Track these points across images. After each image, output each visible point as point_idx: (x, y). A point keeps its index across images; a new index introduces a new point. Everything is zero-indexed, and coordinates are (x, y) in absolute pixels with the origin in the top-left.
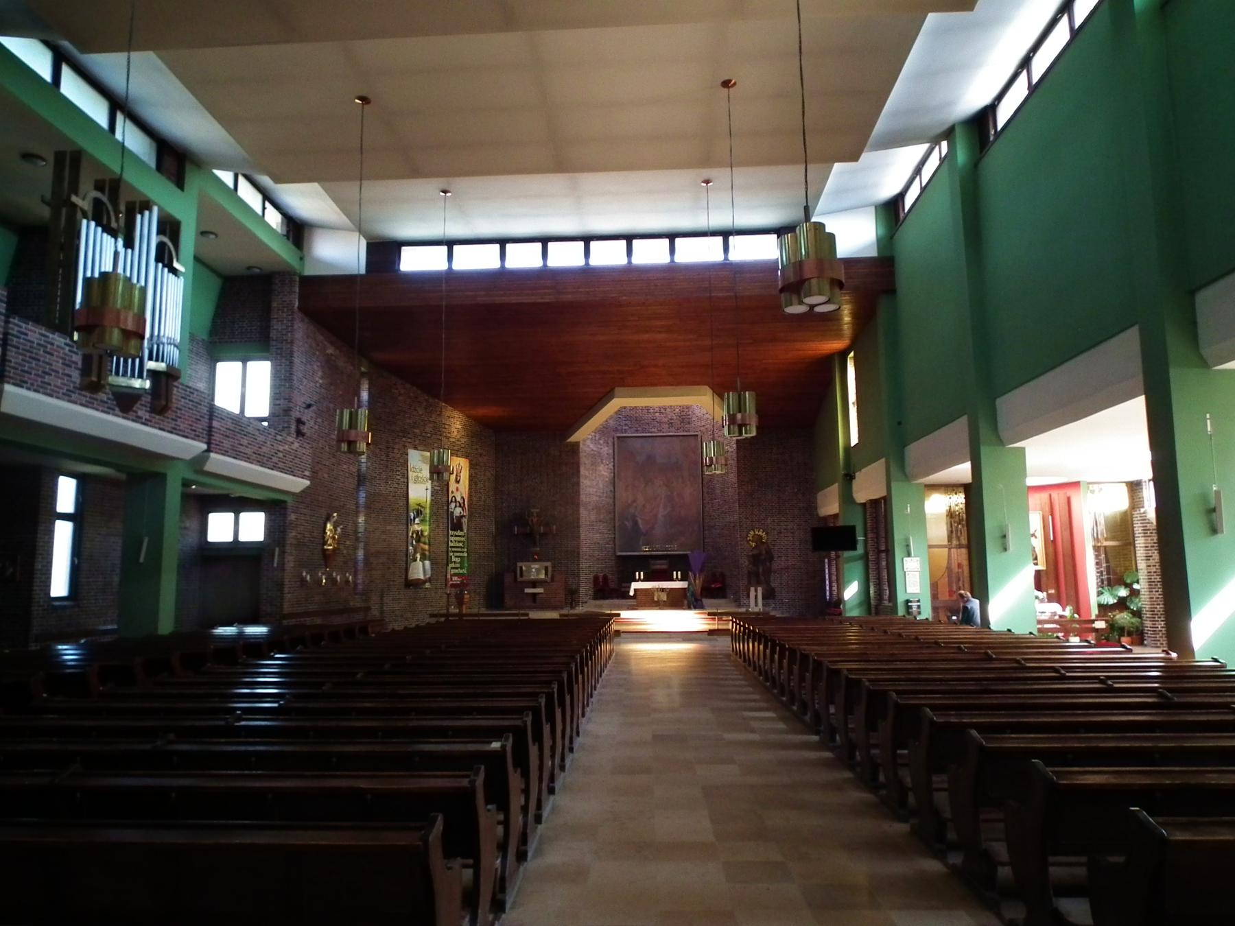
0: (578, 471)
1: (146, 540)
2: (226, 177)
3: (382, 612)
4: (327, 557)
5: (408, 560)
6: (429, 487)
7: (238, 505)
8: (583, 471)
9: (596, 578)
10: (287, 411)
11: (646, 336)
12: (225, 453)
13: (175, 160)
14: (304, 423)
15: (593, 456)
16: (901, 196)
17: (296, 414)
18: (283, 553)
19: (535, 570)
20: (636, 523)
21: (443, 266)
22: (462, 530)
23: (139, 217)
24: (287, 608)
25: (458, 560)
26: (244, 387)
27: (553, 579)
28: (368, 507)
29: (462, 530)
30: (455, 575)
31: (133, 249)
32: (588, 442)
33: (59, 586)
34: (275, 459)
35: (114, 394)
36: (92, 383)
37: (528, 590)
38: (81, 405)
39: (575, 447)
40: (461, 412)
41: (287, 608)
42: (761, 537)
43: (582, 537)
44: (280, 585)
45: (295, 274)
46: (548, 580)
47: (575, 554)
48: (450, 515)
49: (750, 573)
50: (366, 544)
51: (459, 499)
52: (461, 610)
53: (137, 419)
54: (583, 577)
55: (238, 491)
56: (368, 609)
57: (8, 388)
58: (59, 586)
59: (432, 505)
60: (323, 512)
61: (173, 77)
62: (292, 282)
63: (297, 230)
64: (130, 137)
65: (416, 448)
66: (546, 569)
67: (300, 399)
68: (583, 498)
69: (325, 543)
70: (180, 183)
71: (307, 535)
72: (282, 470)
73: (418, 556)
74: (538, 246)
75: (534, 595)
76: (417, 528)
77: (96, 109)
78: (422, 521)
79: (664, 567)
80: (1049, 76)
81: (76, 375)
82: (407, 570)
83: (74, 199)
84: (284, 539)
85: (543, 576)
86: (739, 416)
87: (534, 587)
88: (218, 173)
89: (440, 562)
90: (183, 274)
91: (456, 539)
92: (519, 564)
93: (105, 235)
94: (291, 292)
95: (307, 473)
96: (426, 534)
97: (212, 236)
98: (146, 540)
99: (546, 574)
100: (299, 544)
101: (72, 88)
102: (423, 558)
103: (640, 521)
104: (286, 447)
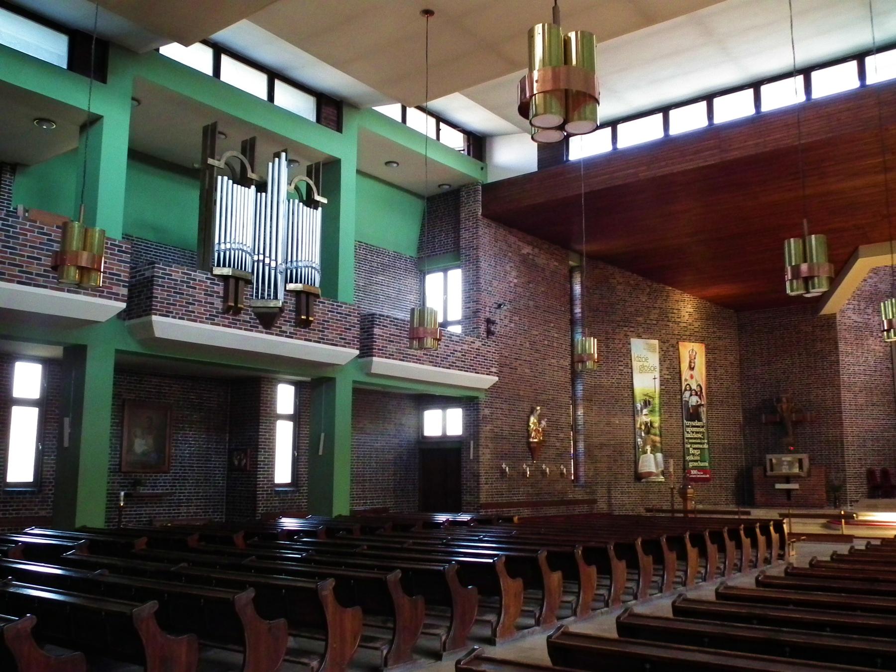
0: (837, 348)
1: (323, 435)
2: (392, 111)
3: (610, 505)
4: (532, 450)
5: (636, 452)
6: (657, 375)
7: (444, 401)
8: (842, 346)
9: (871, 474)
10: (476, 312)
11: (859, 182)
12: (391, 356)
13: (332, 109)
14: (493, 323)
15: (858, 329)
17: (483, 316)
18: (477, 446)
19: (786, 463)
22: (700, 420)
23: (270, 164)
24: (483, 498)
25: (697, 452)
26: (445, 294)
27: (809, 474)
28: (588, 399)
29: (700, 420)
30: (694, 468)
31: (266, 192)
32: (849, 313)
33: (283, 473)
34: (451, 359)
35: (256, 314)
36: (231, 311)
37: (778, 486)
38: (224, 326)
40: (691, 293)
41: (483, 498)
43: (847, 423)
44: (477, 476)
45: (477, 183)
47: (838, 443)
48: (684, 405)
50: (587, 437)
51: (694, 387)
52: (685, 505)
53: (282, 333)
54: (850, 471)
55: (438, 391)
56: (594, 501)
57: (155, 318)
58: (283, 473)
59: (661, 395)
60: (526, 406)
61: (283, 41)
62: (476, 191)
63: (478, 144)
64: (288, 98)
65: (639, 337)
66: (800, 461)
67: (489, 301)
68: (845, 378)
69: (529, 436)
70: (339, 128)
71: (506, 428)
72: (461, 369)
73: (649, 448)
75: (788, 491)
76: (647, 419)
77: (254, 83)
78: (652, 412)
81: (218, 303)
82: (636, 463)
83: (210, 161)
84: (478, 432)
85: (796, 470)
86: (804, 267)
87: (788, 482)
88: (380, 109)
89: (673, 451)
90: (323, 205)
91: (692, 430)
92: (769, 456)
93: (235, 185)
94: (476, 201)
95: (494, 370)
96: (656, 425)
97: (395, 165)
98: (323, 435)
99: (801, 467)
100: (496, 437)
101: (233, 73)
102: (654, 451)
104: (465, 347)
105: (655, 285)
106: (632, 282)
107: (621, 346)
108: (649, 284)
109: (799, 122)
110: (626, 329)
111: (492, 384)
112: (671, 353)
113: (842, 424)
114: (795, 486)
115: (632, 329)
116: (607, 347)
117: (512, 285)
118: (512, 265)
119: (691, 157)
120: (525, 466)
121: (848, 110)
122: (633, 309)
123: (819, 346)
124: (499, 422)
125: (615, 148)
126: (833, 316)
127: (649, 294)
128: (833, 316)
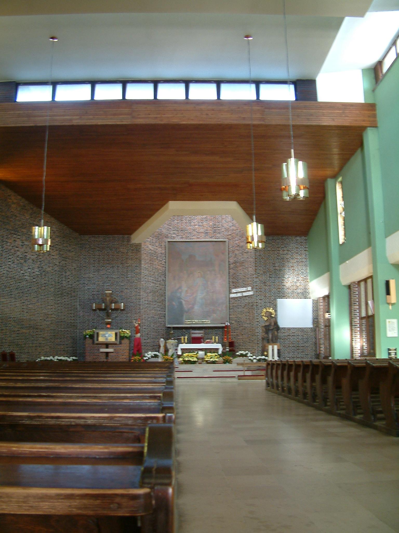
0: (140, 264)
11: (312, 111)
16: (380, 63)
20: (181, 303)
21: (214, 97)
39: (137, 248)
42: (271, 314)
46: (118, 342)
49: (263, 339)
74: (253, 86)
75: (107, 353)
79: (199, 335)
80: (392, 69)
87: (107, 347)
103: (184, 302)
106: (21, 204)
108: (32, 207)
109: (249, 60)
110: (15, 236)
112: (41, 257)
115: (19, 237)
122: (20, 223)
123: (130, 262)
127: (31, 214)
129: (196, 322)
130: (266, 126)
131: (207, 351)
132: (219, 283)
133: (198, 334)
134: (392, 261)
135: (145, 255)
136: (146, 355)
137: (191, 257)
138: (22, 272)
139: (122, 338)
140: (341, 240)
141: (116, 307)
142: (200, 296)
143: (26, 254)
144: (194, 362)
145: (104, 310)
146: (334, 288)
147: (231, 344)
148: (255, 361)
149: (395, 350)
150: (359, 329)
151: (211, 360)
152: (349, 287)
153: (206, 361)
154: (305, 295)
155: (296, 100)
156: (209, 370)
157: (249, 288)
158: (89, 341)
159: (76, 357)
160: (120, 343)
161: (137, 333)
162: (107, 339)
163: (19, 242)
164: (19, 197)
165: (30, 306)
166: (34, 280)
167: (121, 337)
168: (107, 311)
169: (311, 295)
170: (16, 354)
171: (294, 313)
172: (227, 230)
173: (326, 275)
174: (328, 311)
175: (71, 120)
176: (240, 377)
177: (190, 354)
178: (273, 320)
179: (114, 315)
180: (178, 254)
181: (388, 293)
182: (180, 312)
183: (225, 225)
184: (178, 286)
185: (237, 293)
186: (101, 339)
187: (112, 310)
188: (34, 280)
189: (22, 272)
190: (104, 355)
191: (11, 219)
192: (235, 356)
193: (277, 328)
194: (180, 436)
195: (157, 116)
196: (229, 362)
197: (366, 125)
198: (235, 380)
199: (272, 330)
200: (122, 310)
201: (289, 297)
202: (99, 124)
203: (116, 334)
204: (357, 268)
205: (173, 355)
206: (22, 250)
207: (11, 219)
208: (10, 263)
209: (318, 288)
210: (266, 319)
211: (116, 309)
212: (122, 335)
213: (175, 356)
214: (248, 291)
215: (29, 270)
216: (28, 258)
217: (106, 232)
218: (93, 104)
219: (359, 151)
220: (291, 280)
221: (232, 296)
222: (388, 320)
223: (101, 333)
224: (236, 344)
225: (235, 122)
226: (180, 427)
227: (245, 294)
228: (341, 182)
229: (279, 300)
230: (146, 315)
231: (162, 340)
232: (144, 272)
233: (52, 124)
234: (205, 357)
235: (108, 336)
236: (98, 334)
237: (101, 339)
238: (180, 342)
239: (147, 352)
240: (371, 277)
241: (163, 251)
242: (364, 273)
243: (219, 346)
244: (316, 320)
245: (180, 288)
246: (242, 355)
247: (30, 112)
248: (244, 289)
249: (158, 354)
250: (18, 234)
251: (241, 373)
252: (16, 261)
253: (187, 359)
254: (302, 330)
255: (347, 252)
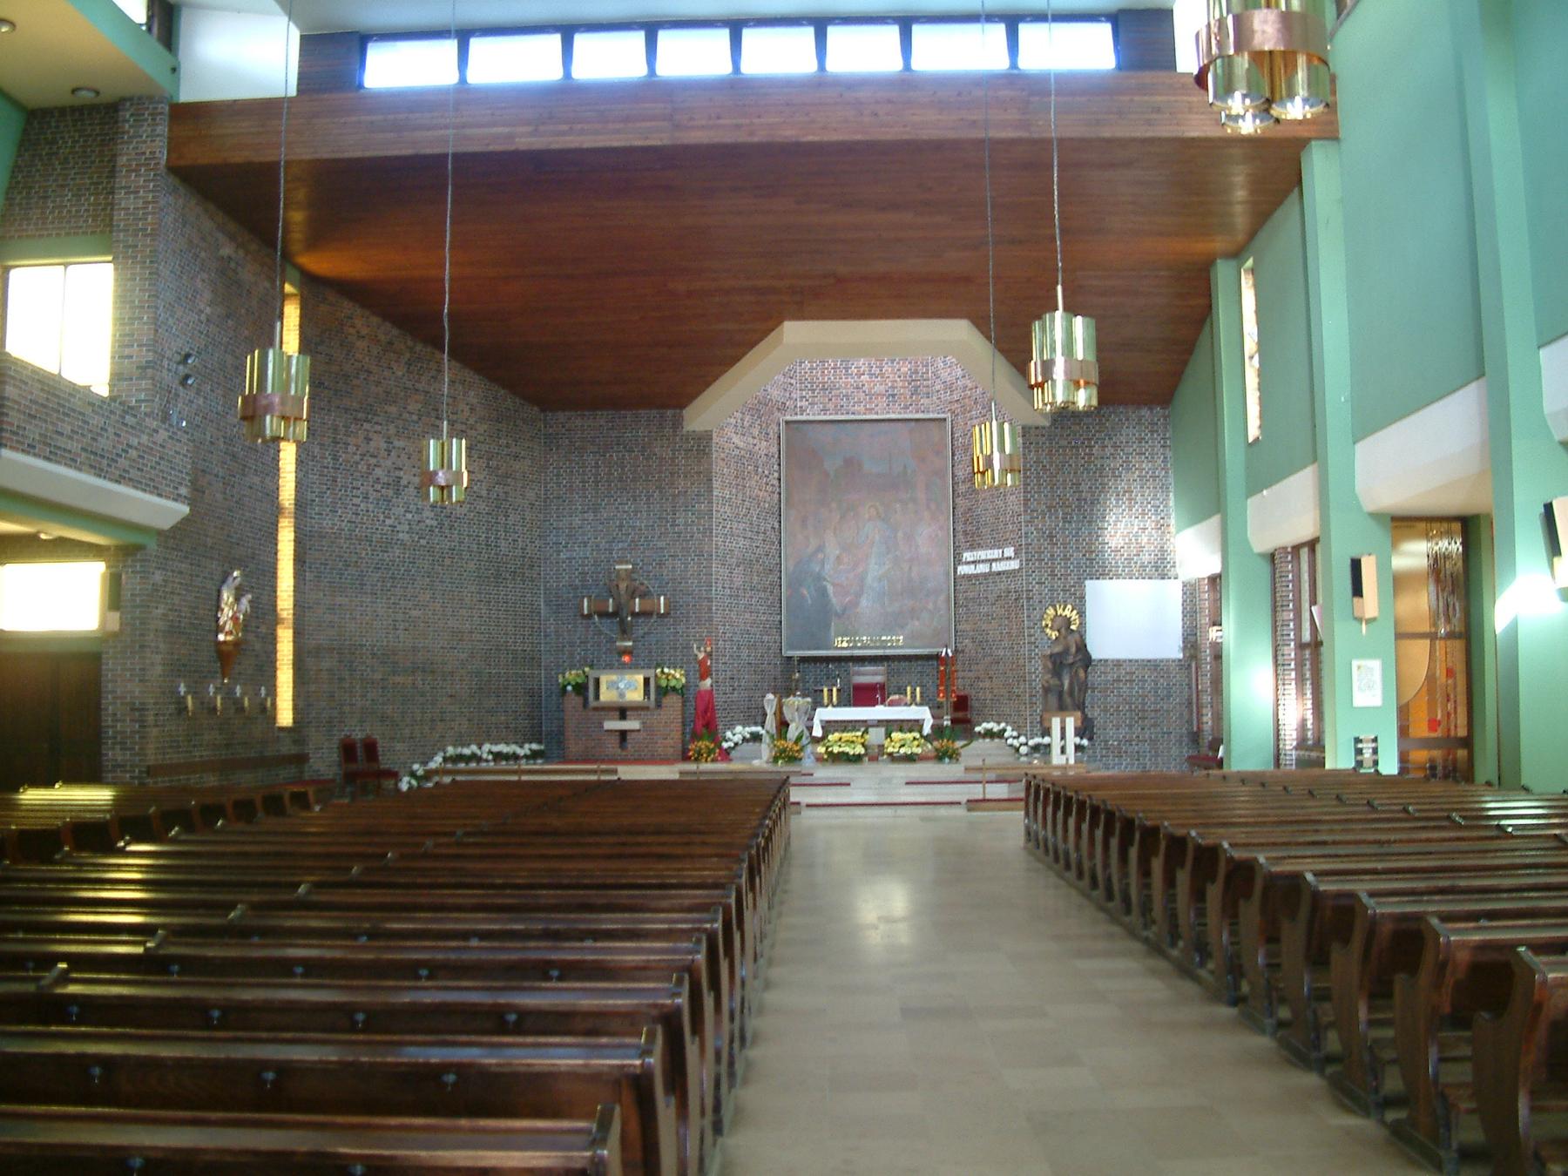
0: (710, 489)
11: (1160, 98)
12: (29, 449)
20: (823, 592)
39: (701, 444)
42: (1068, 621)
75: (623, 734)
79: (879, 679)
103: (830, 589)
105: (419, 347)
107: (357, 458)
108: (410, 343)
111: (178, 519)
113: (710, 619)
114: (630, 724)
115: (378, 428)
116: (335, 458)
117: (203, 317)
118: (205, 276)
119: (617, 126)
120: (212, 689)
121: (889, 101)
123: (681, 483)
124: (176, 600)
125: (463, 79)
126: (707, 436)
127: (409, 364)
128: (707, 436)
129: (865, 643)
130: (1034, 142)
131: (890, 726)
132: (928, 536)
133: (870, 675)
134: (1370, 505)
135: (721, 463)
136: (729, 734)
137: (852, 465)
138: (388, 522)
139: (663, 692)
140: (1253, 432)
141: (648, 608)
142: (875, 570)
143: (397, 473)
144: (857, 759)
145: (615, 614)
146: (1231, 561)
147: (962, 704)
148: (1023, 750)
149: (1375, 740)
150: (1293, 674)
151: (902, 751)
152: (1272, 556)
153: (890, 754)
154: (1160, 568)
155: (1119, 67)
156: (892, 782)
157: (1010, 552)
158: (573, 701)
159: (540, 742)
160: (659, 705)
161: (703, 678)
162: (622, 695)
163: (379, 443)
164: (375, 320)
165: (414, 613)
166: (423, 542)
167: (658, 687)
168: (621, 620)
169: (1178, 570)
170: (380, 743)
171: (1130, 619)
172: (950, 387)
173: (1215, 520)
174: (1217, 622)
175: (511, 137)
176: (973, 804)
177: (846, 736)
178: (1072, 641)
179: (641, 628)
180: (813, 456)
181: (1357, 590)
182: (822, 617)
183: (944, 375)
184: (814, 543)
185: (978, 561)
186: (606, 695)
187: (634, 614)
188: (423, 542)
189: (388, 522)
190: (615, 739)
191: (355, 382)
192: (971, 736)
193: (1087, 661)
194: (771, 997)
195: (739, 121)
196: (952, 756)
197: (1306, 134)
198: (960, 812)
199: (1071, 673)
200: (661, 616)
201: (1118, 576)
202: (585, 146)
203: (647, 681)
204: (1284, 514)
205: (799, 738)
206: (389, 463)
207: (355, 382)
208: (355, 501)
209: (1196, 553)
210: (1054, 635)
211: (645, 614)
212: (664, 683)
213: (804, 741)
214: (1000, 559)
215: (409, 516)
216: (403, 482)
217: (616, 404)
218: (566, 97)
219: (1296, 190)
220: (1121, 528)
221: (963, 570)
222: (1355, 663)
223: (604, 679)
224: (975, 704)
225: (951, 135)
226: (775, 973)
227: (997, 567)
228: (1252, 271)
229: (1090, 585)
230: (729, 627)
231: (770, 696)
232: (721, 511)
233: (461, 149)
234: (887, 743)
235: (624, 686)
236: (597, 681)
237: (606, 695)
238: (818, 703)
239: (731, 727)
240: (1312, 545)
241: (774, 449)
242: (1304, 529)
243: (924, 714)
244: (1192, 639)
245: (820, 549)
246: (989, 734)
247: (401, 116)
248: (996, 553)
249: (763, 732)
250: (379, 419)
251: (976, 792)
252: (373, 495)
253: (836, 750)
254: (1154, 666)
255: (1267, 467)
